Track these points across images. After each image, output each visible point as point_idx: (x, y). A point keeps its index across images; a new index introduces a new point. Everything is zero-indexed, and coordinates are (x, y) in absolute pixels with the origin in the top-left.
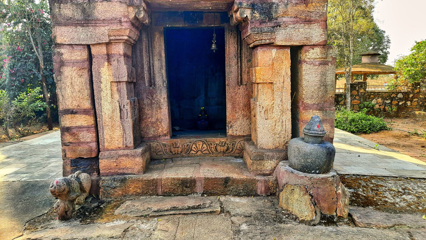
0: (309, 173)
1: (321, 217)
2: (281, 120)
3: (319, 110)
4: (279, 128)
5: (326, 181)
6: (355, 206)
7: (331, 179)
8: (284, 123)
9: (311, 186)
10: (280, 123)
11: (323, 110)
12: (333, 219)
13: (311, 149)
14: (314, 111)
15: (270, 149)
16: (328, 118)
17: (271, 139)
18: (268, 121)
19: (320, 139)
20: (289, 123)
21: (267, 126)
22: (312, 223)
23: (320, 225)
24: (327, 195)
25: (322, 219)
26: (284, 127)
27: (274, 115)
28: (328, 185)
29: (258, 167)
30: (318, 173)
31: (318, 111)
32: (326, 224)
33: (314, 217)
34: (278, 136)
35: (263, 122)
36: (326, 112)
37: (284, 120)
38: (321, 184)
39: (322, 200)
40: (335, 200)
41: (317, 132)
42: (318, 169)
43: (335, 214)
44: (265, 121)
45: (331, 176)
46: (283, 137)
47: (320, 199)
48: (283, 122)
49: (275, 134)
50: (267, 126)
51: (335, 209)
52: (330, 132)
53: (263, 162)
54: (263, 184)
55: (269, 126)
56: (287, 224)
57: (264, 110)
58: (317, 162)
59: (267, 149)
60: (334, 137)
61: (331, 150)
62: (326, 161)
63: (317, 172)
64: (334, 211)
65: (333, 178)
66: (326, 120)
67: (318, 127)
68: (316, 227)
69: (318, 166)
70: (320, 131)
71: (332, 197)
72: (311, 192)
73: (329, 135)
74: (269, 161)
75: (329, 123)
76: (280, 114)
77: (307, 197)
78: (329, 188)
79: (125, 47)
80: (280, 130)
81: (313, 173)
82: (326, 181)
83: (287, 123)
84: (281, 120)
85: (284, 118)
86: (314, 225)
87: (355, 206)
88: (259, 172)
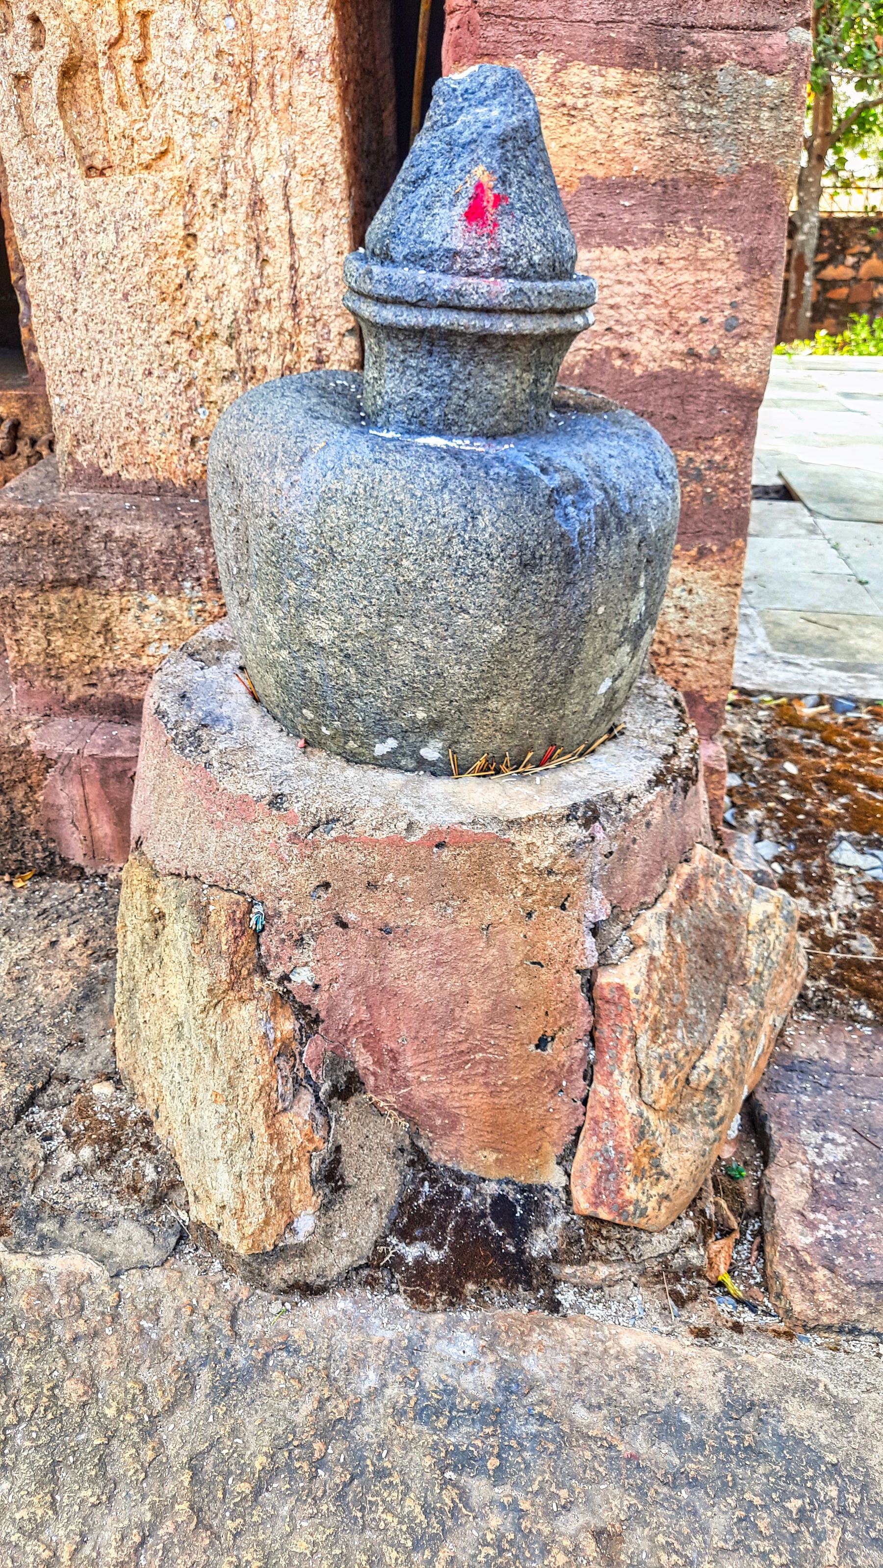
0: (352, 759)
1: (405, 1203)
2: (240, 186)
3: (634, 59)
4: (226, 275)
5: (482, 864)
6: (853, 1019)
7: (545, 846)
8: (274, 219)
9: (313, 912)
10: (232, 222)
11: (674, 63)
12: (519, 1229)
13: (328, 498)
14: (578, 74)
15: (161, 489)
16: (723, 161)
17: (161, 388)
18: (110, 192)
19: (505, 382)
20: (327, 219)
21: (106, 241)
22: (283, 1272)
23: (371, 1283)
24: (478, 1007)
25: (410, 1220)
26: (279, 257)
27: (164, 120)
28: (497, 909)
29: (58, 641)
30: (436, 770)
31: (614, 76)
32: (422, 1284)
33: (306, 1223)
34: (225, 356)
35: (62, 201)
36: (708, 82)
37: (270, 185)
38: (428, 899)
39: (425, 1045)
40: (566, 1052)
41: (442, 283)
42: (435, 725)
43: (555, 1177)
44: (82, 188)
45: (561, 803)
46: (274, 366)
47: (399, 1034)
48: (257, 206)
49: (195, 336)
50: (106, 241)
51: (558, 1133)
52: (729, 326)
53: (102, 606)
54: (93, 791)
55: (132, 244)
56: (47, 1244)
57: (55, 53)
58: (404, 658)
59: (144, 490)
60: (764, 375)
61: (577, 519)
62: (501, 655)
63: (431, 752)
64: (553, 1152)
65: (574, 831)
66: (705, 181)
67: (475, 213)
68: (315, 1313)
69: (415, 692)
70: (503, 271)
71: (531, 1026)
72: (302, 977)
73: (716, 357)
74: (152, 599)
75: (728, 217)
76: (219, 107)
77: (249, 1021)
78: (515, 933)
79: (360, 120)
80: (235, 298)
81: (387, 763)
82: (482, 864)
83: (303, 222)
84: (240, 186)
85: (267, 155)
86: (310, 1290)
87: (853, 1019)
88: (79, 690)
